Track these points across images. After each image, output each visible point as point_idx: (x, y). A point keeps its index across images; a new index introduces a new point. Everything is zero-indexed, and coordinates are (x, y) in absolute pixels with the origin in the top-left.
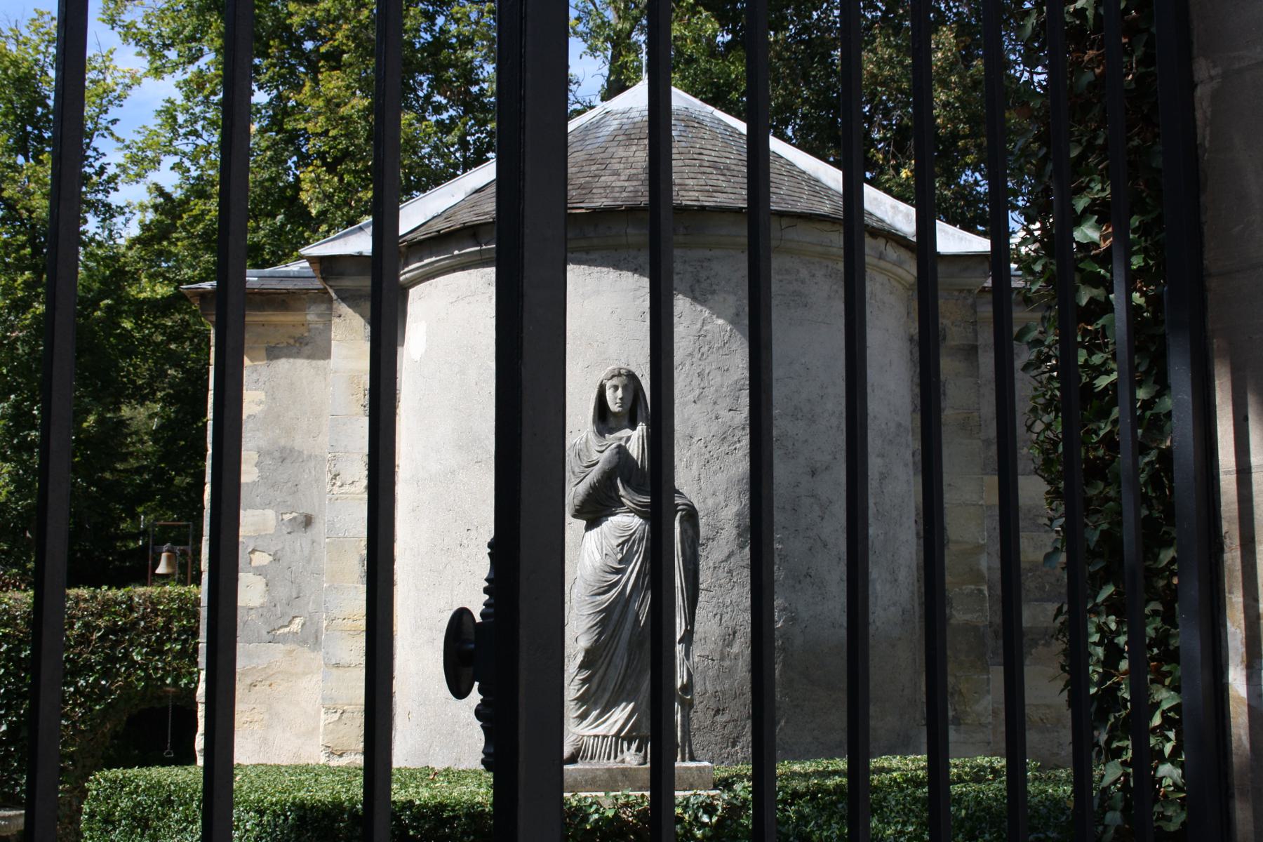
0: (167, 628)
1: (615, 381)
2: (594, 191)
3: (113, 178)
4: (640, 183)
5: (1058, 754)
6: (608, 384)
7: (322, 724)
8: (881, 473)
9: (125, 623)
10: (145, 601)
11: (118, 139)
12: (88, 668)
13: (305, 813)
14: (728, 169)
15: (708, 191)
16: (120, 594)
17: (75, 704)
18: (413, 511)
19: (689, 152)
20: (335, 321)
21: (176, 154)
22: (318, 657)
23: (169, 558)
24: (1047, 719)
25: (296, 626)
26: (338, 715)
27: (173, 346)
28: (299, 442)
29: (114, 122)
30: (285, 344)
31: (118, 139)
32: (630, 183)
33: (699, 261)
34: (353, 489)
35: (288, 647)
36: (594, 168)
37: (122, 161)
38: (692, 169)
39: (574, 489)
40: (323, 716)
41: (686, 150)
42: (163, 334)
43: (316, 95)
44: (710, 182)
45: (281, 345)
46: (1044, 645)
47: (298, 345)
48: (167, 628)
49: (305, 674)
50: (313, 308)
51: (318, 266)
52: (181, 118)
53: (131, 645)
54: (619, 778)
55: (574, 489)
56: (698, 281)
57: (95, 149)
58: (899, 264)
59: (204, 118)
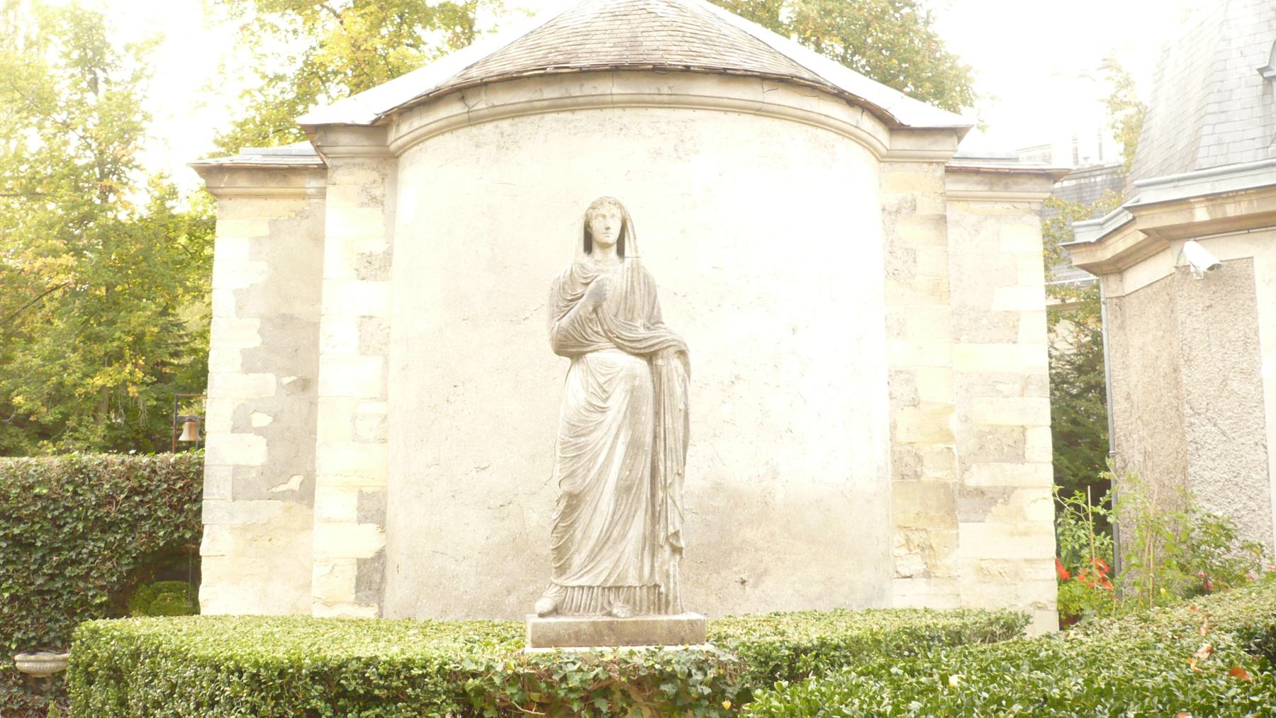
2: (580, 55)
4: (625, 48)
5: (1015, 605)
13: (258, 671)
15: (692, 56)
16: (144, 459)
18: (403, 369)
19: (672, 25)
23: (190, 427)
24: (1005, 572)
30: (287, 217)
32: (615, 49)
33: (683, 122)
35: (287, 504)
39: (558, 323)
41: (669, 24)
45: (282, 218)
46: (1002, 503)
47: (299, 218)
54: (606, 632)
55: (558, 323)
56: (682, 141)
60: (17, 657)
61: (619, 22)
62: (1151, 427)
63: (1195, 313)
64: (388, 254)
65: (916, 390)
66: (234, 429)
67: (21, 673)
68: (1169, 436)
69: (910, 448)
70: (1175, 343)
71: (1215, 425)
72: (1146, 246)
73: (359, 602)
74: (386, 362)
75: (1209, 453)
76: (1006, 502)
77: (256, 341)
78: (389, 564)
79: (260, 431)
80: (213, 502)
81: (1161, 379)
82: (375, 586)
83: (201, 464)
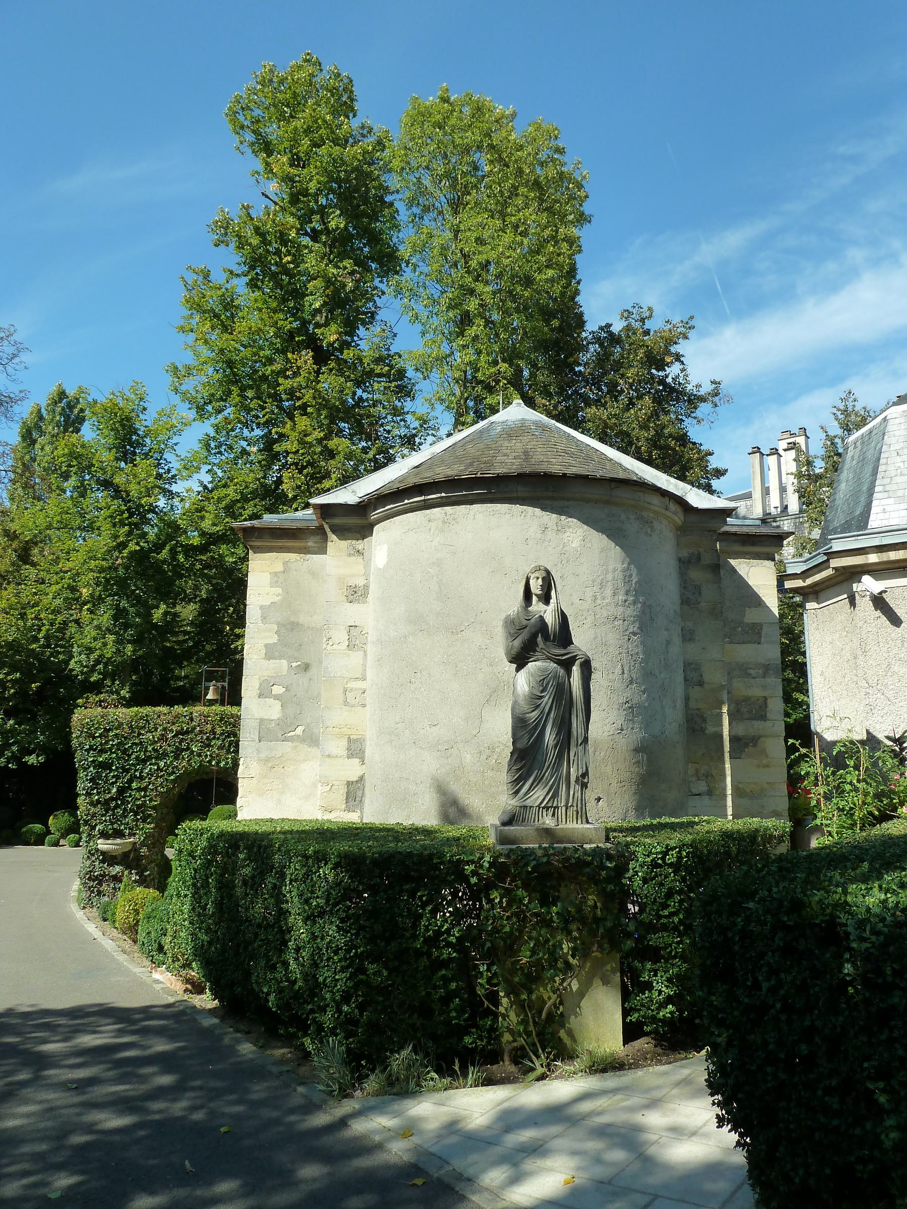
0: (213, 732)
1: (537, 574)
3: (174, 476)
6: (532, 576)
7: (319, 792)
8: (667, 641)
9: (188, 728)
10: (200, 715)
11: (177, 456)
12: (165, 755)
14: (574, 454)
17: (157, 777)
20: (329, 544)
21: (210, 464)
22: (315, 751)
25: (299, 731)
26: (329, 786)
27: (206, 571)
28: (303, 619)
29: (176, 444)
31: (177, 456)
34: (339, 647)
36: (491, 452)
37: (179, 467)
38: (553, 453)
40: (320, 788)
42: (201, 565)
43: (293, 428)
44: (565, 461)
48: (213, 732)
49: (304, 761)
50: (312, 538)
51: (318, 511)
52: (213, 445)
53: (192, 741)
57: (165, 459)
58: (675, 513)
59: (226, 445)
60: (99, 841)
61: (514, 441)
62: (839, 694)
63: (869, 621)
64: (366, 587)
65: (701, 675)
66: (260, 696)
67: (102, 852)
68: (851, 700)
69: (698, 712)
70: (855, 641)
71: (883, 694)
72: (835, 577)
73: (348, 809)
74: (365, 655)
75: (879, 712)
76: (755, 745)
77: (274, 639)
78: (367, 785)
79: (277, 697)
80: (246, 743)
81: (845, 663)
82: (358, 799)
83: (239, 717)
